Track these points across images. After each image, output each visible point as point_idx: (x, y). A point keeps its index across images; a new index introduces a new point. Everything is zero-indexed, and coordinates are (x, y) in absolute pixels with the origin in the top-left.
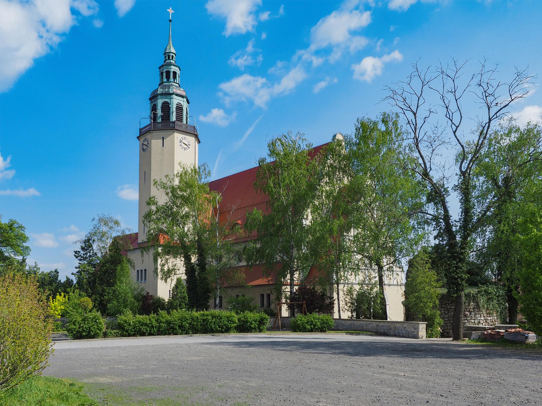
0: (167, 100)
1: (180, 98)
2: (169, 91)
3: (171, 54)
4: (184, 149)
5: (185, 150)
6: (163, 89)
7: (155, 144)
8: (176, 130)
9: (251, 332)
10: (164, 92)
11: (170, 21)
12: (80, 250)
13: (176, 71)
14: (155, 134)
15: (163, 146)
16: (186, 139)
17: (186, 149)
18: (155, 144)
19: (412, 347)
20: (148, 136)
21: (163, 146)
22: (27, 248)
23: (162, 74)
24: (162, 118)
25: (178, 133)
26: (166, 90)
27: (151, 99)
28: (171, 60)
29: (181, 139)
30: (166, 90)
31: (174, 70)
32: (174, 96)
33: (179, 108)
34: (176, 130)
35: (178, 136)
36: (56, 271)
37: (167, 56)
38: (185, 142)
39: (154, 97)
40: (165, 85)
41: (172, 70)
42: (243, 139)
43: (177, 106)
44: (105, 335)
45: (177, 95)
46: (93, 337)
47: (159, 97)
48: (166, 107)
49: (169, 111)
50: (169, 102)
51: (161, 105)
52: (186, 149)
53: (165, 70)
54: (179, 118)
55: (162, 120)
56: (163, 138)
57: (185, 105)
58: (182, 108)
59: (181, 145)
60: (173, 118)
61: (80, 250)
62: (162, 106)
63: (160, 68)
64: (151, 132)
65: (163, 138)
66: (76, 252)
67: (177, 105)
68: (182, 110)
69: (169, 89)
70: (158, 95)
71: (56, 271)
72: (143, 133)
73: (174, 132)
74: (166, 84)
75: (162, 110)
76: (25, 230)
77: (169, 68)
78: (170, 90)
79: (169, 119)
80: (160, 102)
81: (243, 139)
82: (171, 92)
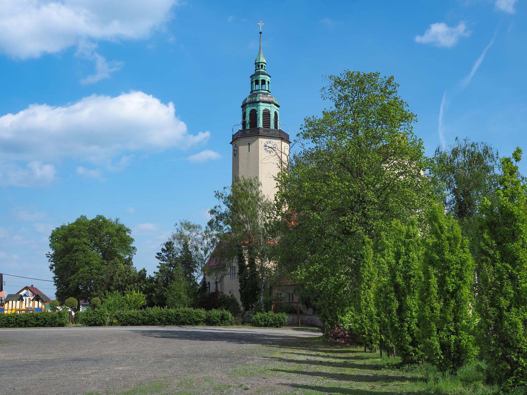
0: (254, 108)
1: (267, 104)
2: (256, 99)
3: (261, 64)
4: (269, 152)
5: (270, 153)
6: (251, 98)
7: (243, 149)
8: (260, 135)
9: (216, 325)
10: (251, 101)
11: (261, 33)
12: (161, 252)
13: (264, 79)
14: (242, 140)
15: (249, 151)
16: (271, 142)
17: (271, 152)
18: (243, 149)
19: (114, 332)
20: (237, 143)
21: (249, 151)
22: (134, 248)
23: (252, 82)
24: (250, 124)
25: (262, 138)
26: (254, 99)
27: (242, 107)
28: (260, 69)
29: (266, 143)
30: (254, 99)
31: (262, 79)
32: (261, 104)
33: (267, 114)
34: (260, 135)
35: (262, 141)
36: (144, 270)
37: (258, 65)
38: (270, 146)
39: (244, 106)
40: (254, 93)
41: (261, 79)
42: (472, 74)
43: (263, 113)
44: (111, 324)
45: (264, 102)
46: (100, 325)
47: (248, 106)
48: (254, 114)
49: (256, 118)
50: (256, 109)
51: (249, 113)
52: (271, 152)
53: (254, 80)
54: (267, 123)
55: (250, 126)
56: (249, 143)
57: (273, 109)
58: (270, 113)
59: (265, 149)
60: (261, 125)
61: (161, 252)
62: (250, 113)
63: (251, 77)
64: (239, 139)
65: (249, 143)
66: (158, 254)
67: (264, 112)
68: (270, 115)
69: (256, 97)
70: (246, 104)
71: (144, 270)
72: (236, 139)
73: (258, 138)
74: (255, 92)
75: (250, 117)
76: (132, 233)
77: (258, 77)
78: (257, 98)
79: (256, 126)
80: (248, 110)
81: (472, 74)
82: (258, 100)
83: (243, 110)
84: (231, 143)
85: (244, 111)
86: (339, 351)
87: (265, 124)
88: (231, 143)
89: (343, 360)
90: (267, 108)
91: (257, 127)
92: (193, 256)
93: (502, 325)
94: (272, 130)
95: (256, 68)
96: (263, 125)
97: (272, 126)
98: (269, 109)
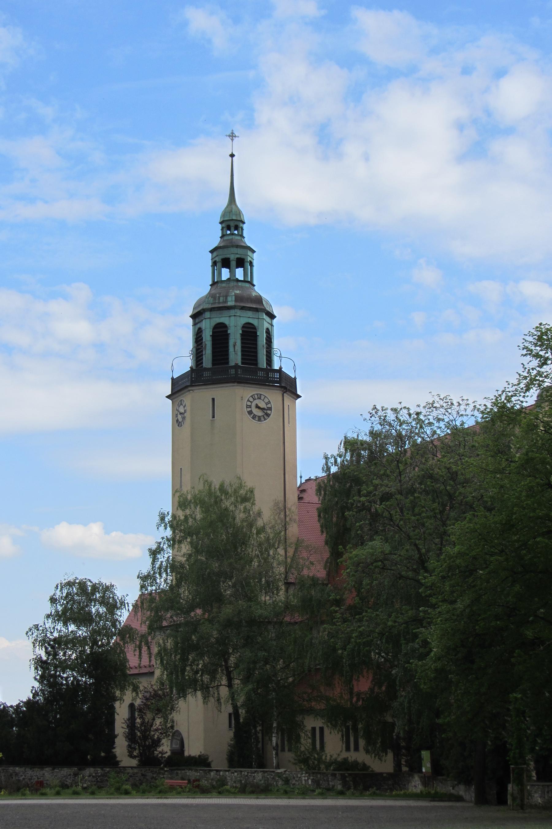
1: (250, 314)
4: (257, 419)
16: (262, 397)
23: (214, 264)
58: (256, 333)
62: (213, 332)
63: (212, 252)
80: (207, 326)
83: (195, 324)
84: (168, 397)
85: (198, 326)
86: (320, 740)
87: (247, 359)
88: (168, 397)
89: (286, 743)
90: (251, 321)
91: (228, 363)
92: (342, 719)
93: (465, 610)
94: (262, 370)
95: (222, 232)
96: (242, 359)
97: (263, 363)
98: (255, 322)
